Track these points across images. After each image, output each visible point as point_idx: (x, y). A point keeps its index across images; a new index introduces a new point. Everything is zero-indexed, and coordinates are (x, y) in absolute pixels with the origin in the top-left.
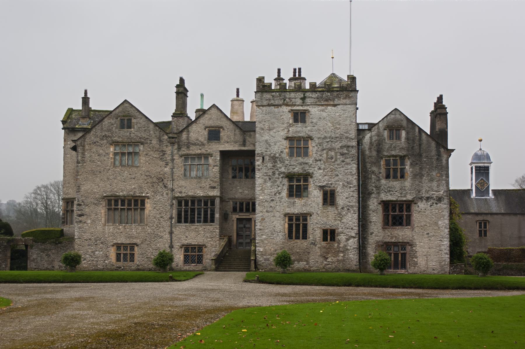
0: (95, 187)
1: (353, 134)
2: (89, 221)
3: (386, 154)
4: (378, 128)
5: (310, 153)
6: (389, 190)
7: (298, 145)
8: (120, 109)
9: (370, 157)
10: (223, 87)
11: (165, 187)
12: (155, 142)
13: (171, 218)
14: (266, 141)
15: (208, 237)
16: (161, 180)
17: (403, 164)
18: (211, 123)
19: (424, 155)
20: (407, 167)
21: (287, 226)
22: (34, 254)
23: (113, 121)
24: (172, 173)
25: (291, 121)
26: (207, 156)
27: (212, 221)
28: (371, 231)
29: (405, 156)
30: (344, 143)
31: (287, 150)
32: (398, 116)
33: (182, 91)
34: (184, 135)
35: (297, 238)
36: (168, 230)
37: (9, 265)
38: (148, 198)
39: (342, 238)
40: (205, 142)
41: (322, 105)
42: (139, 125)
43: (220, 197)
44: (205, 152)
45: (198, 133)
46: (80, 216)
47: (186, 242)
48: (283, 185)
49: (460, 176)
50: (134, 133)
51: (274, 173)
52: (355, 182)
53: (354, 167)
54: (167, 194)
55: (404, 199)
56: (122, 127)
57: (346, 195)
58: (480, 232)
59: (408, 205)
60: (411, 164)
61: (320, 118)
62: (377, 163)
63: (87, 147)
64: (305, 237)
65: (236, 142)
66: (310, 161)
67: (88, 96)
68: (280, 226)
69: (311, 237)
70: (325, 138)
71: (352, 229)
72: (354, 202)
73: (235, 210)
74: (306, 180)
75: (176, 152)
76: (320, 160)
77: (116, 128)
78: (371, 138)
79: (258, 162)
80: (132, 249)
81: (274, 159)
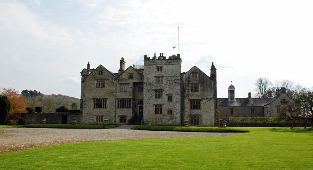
0: (90, 95)
1: (179, 75)
2: (87, 107)
3: (191, 82)
4: (189, 73)
5: (163, 82)
6: (192, 96)
7: (159, 79)
8: (99, 68)
9: (185, 83)
10: (135, 60)
11: (114, 95)
12: (110, 79)
13: (115, 106)
14: (147, 78)
15: (128, 113)
16: (112, 92)
17: (197, 86)
18: (130, 72)
19: (205, 83)
20: (199, 87)
21: (154, 109)
22: (69, 118)
23: (96, 72)
24: (116, 90)
25: (156, 71)
26: (128, 84)
27: (130, 107)
28: (185, 111)
29: (198, 83)
30: (176, 78)
31: (155, 81)
32: (196, 69)
33: (122, 62)
34: (120, 77)
35: (158, 113)
36: (114, 110)
37: (61, 122)
38: (108, 99)
39: (175, 113)
40: (128, 79)
41: (168, 65)
42: (105, 73)
43: (133, 99)
44: (127, 83)
45: (125, 76)
46: (85, 105)
47: (120, 115)
48: (153, 94)
49: (222, 93)
50: (103, 76)
51: (150, 89)
52: (179, 93)
53: (179, 87)
54: (114, 98)
55: (198, 99)
56: (99, 74)
57: (176, 97)
58: (231, 112)
59: (199, 101)
60: (200, 86)
61: (167, 69)
62: (188, 86)
63: (87, 81)
64: (161, 113)
65: (138, 79)
66: (163, 85)
67: (90, 64)
68: (153, 109)
69: (163, 113)
70: (169, 76)
71: (178, 110)
72: (179, 100)
73: (139, 104)
74: (162, 92)
75: (117, 82)
76: (167, 85)
77: (97, 74)
78: (186, 76)
79: (144, 86)
80: (102, 117)
81: (150, 84)
